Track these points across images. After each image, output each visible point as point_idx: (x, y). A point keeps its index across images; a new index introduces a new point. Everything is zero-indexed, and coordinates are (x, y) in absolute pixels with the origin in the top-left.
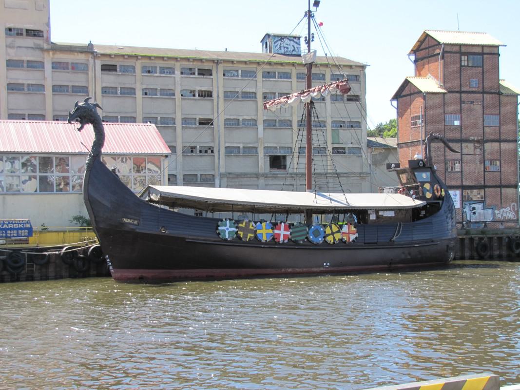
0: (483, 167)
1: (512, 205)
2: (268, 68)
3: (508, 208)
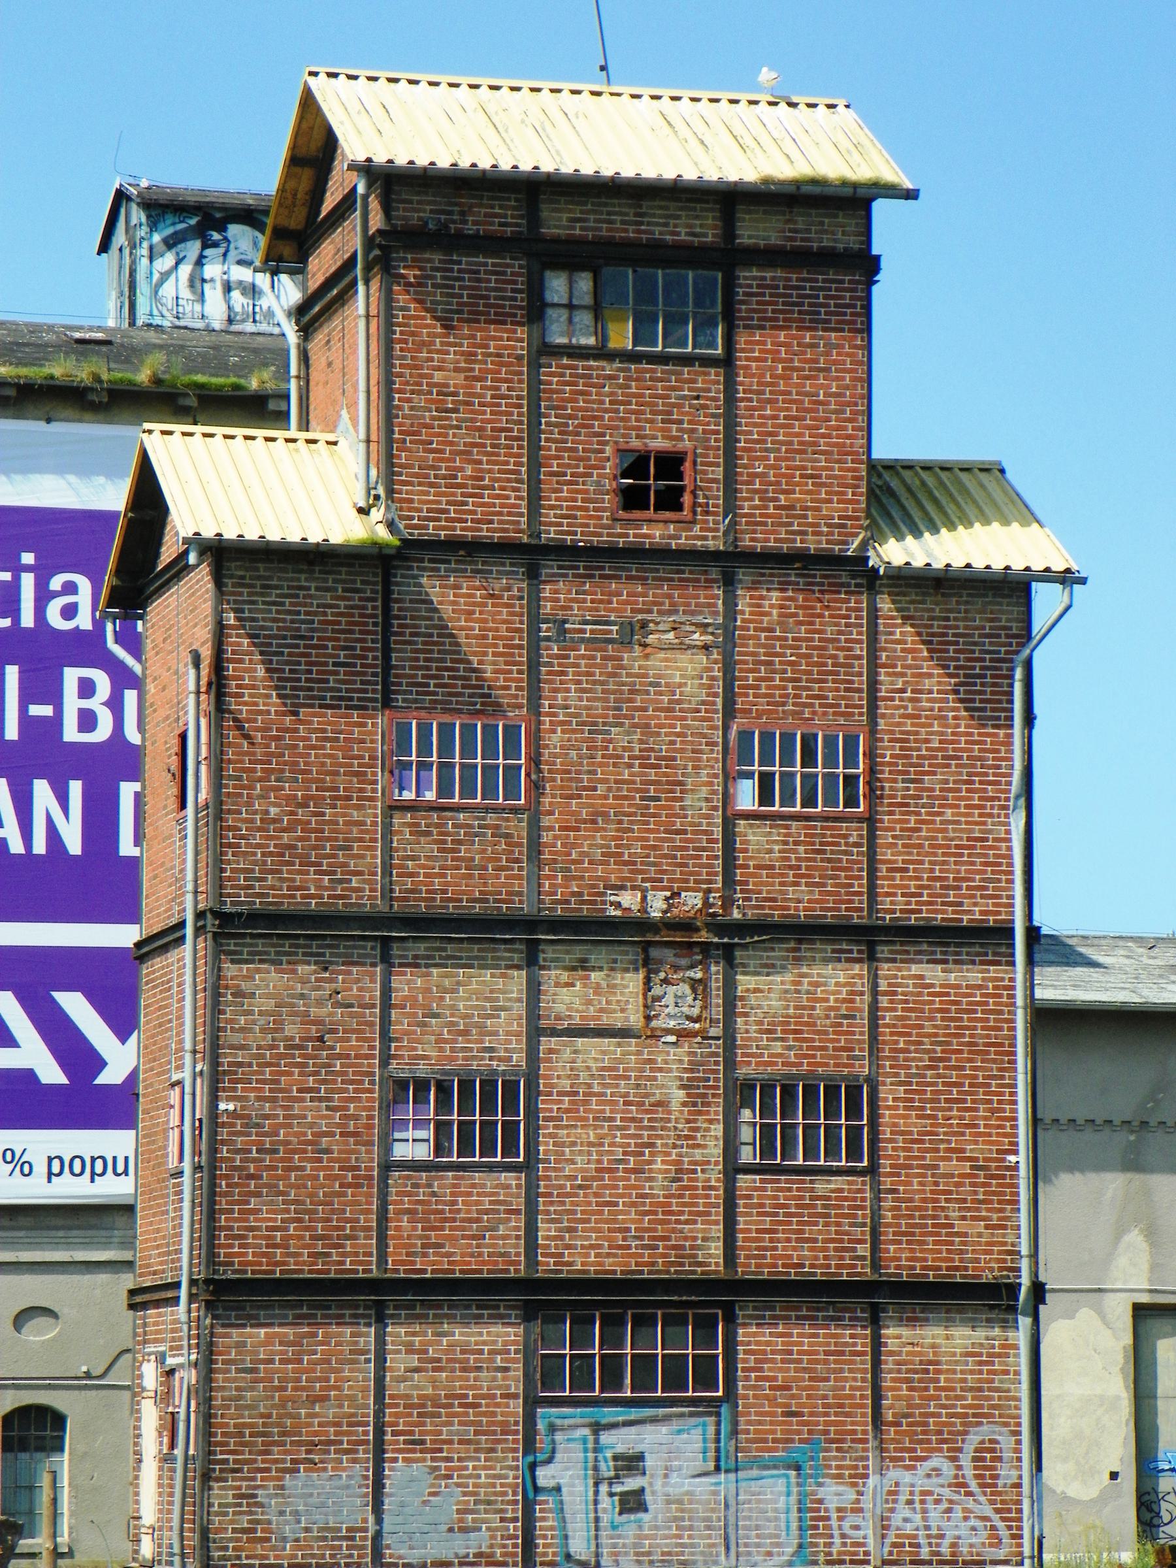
0: (718, 1130)
1: (973, 1440)
2: (733, 756)
3: (936, 1461)
